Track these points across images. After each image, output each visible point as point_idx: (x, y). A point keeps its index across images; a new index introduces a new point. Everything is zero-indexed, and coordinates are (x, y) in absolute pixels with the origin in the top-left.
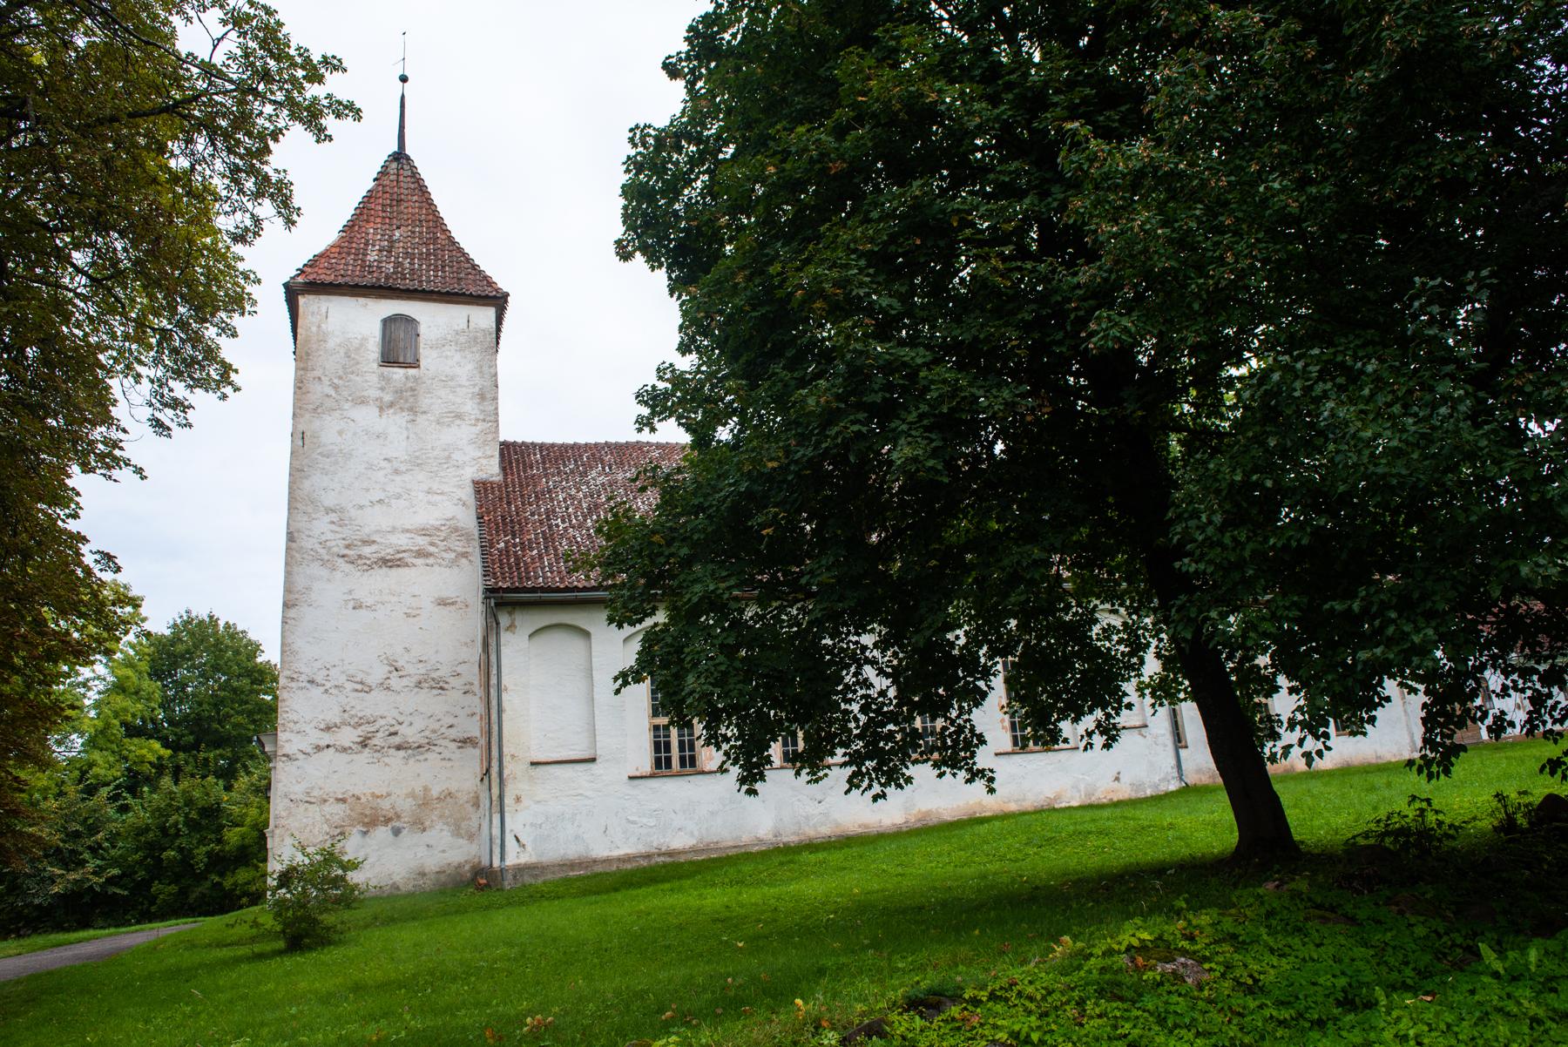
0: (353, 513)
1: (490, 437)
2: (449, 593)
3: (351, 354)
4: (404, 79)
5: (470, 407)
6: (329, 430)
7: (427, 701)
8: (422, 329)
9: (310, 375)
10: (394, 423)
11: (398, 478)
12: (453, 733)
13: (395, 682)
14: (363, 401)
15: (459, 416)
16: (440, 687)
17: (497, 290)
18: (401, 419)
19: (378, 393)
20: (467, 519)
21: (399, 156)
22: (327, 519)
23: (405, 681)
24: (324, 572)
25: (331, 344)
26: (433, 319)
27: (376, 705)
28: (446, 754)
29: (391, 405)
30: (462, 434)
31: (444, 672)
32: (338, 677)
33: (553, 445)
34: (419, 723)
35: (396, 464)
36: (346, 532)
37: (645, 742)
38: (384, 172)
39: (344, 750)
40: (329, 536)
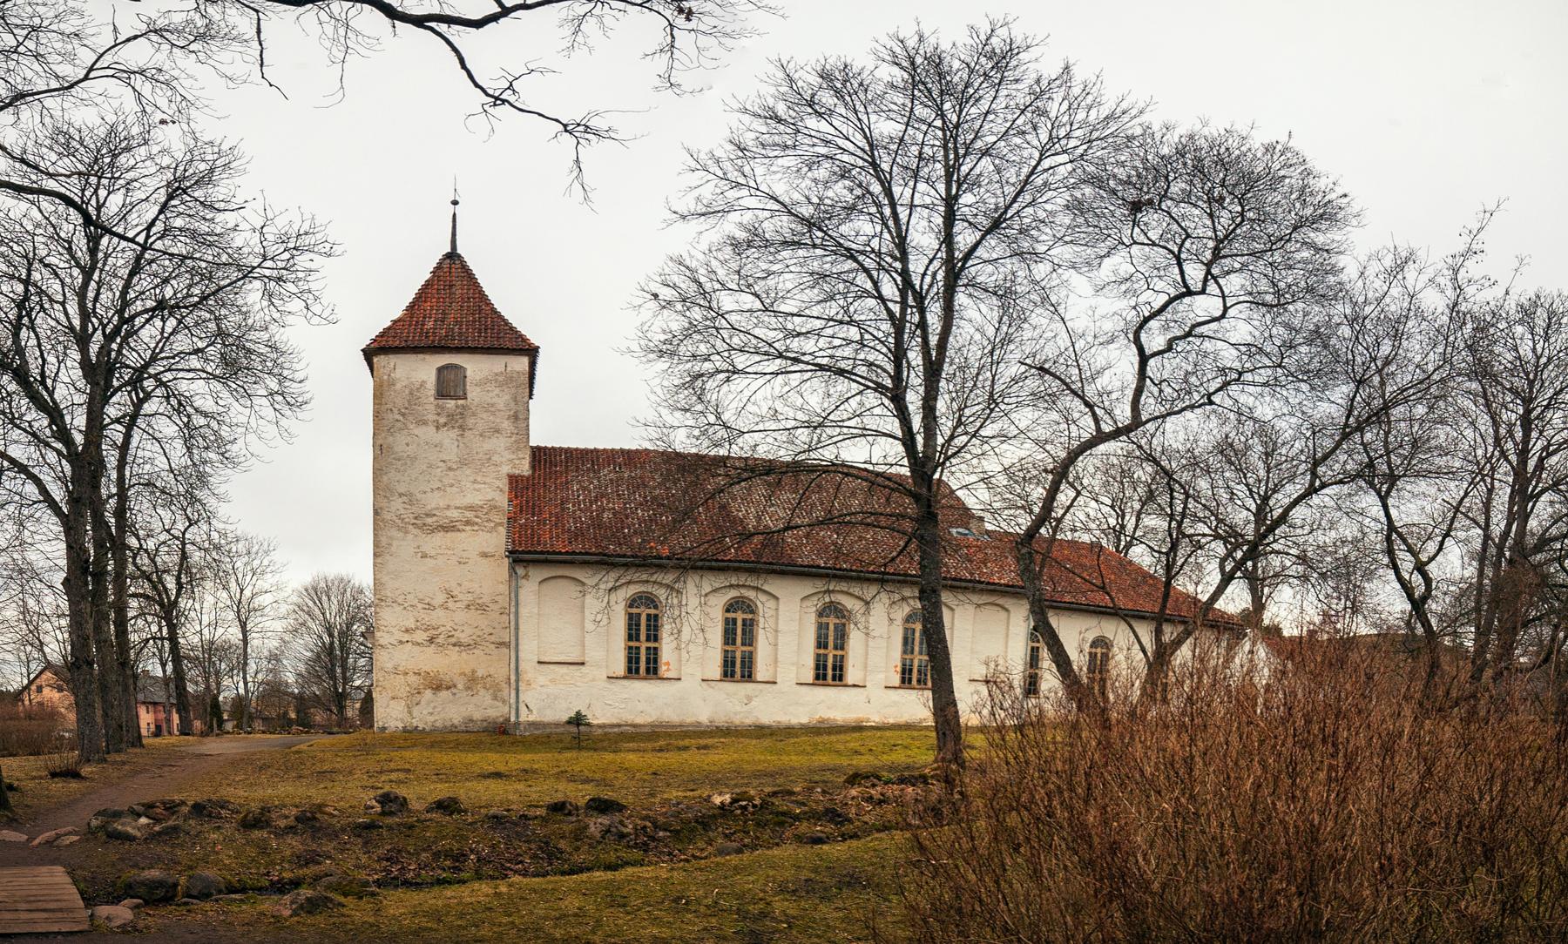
0: (419, 496)
1: (522, 445)
2: (490, 550)
3: (414, 393)
4: (455, 203)
5: (506, 425)
6: (400, 442)
7: (474, 616)
8: (469, 373)
9: (384, 408)
10: (448, 437)
11: (451, 474)
12: (493, 638)
13: (451, 604)
14: (425, 423)
15: (498, 431)
16: (483, 608)
17: (530, 345)
18: (454, 434)
19: (435, 417)
20: (502, 500)
21: (452, 256)
22: (400, 500)
23: (458, 605)
24: (401, 534)
25: (398, 386)
26: (476, 367)
27: (439, 617)
28: (487, 651)
29: (445, 425)
30: (499, 444)
31: (486, 599)
32: (412, 599)
33: (577, 450)
34: (469, 631)
35: (449, 464)
36: (414, 509)
37: (810, 663)
38: (439, 267)
39: (418, 644)
40: (402, 511)
